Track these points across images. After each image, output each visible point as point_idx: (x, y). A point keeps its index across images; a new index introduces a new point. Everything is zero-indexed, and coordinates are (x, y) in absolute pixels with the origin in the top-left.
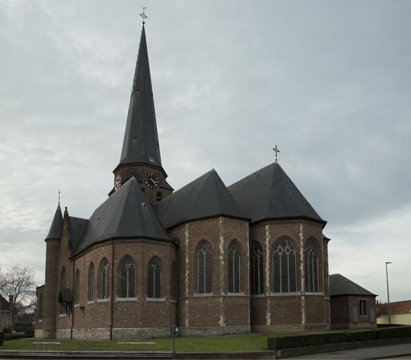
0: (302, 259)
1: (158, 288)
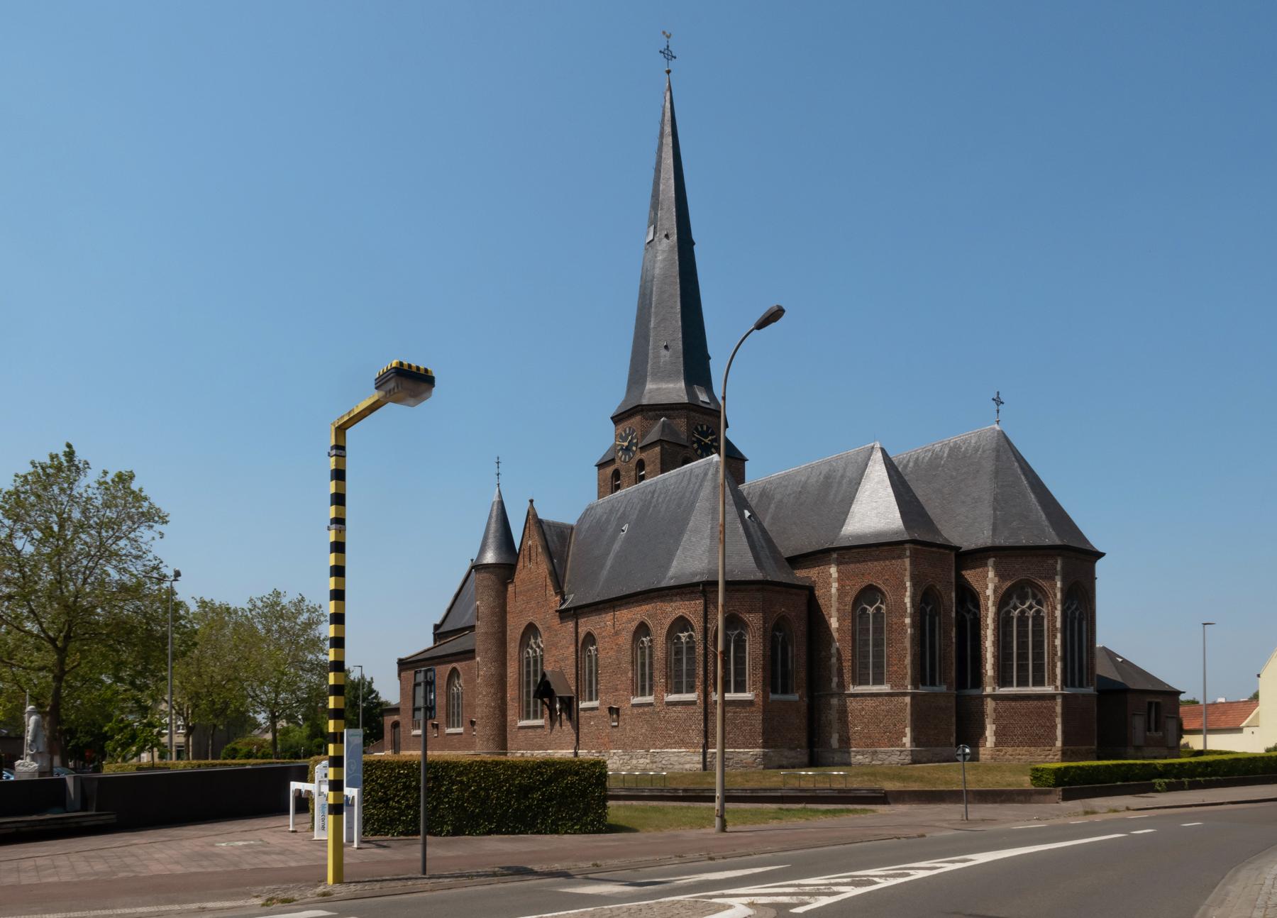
0: (1059, 625)
1: (785, 675)
